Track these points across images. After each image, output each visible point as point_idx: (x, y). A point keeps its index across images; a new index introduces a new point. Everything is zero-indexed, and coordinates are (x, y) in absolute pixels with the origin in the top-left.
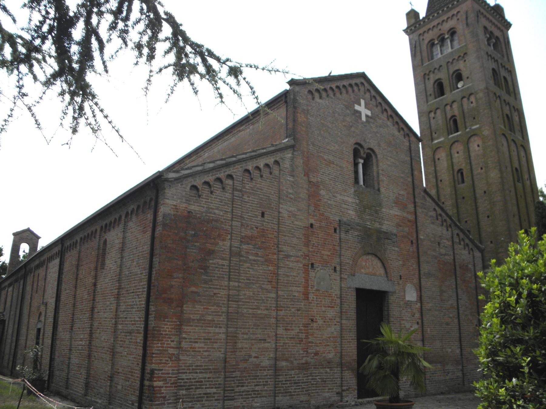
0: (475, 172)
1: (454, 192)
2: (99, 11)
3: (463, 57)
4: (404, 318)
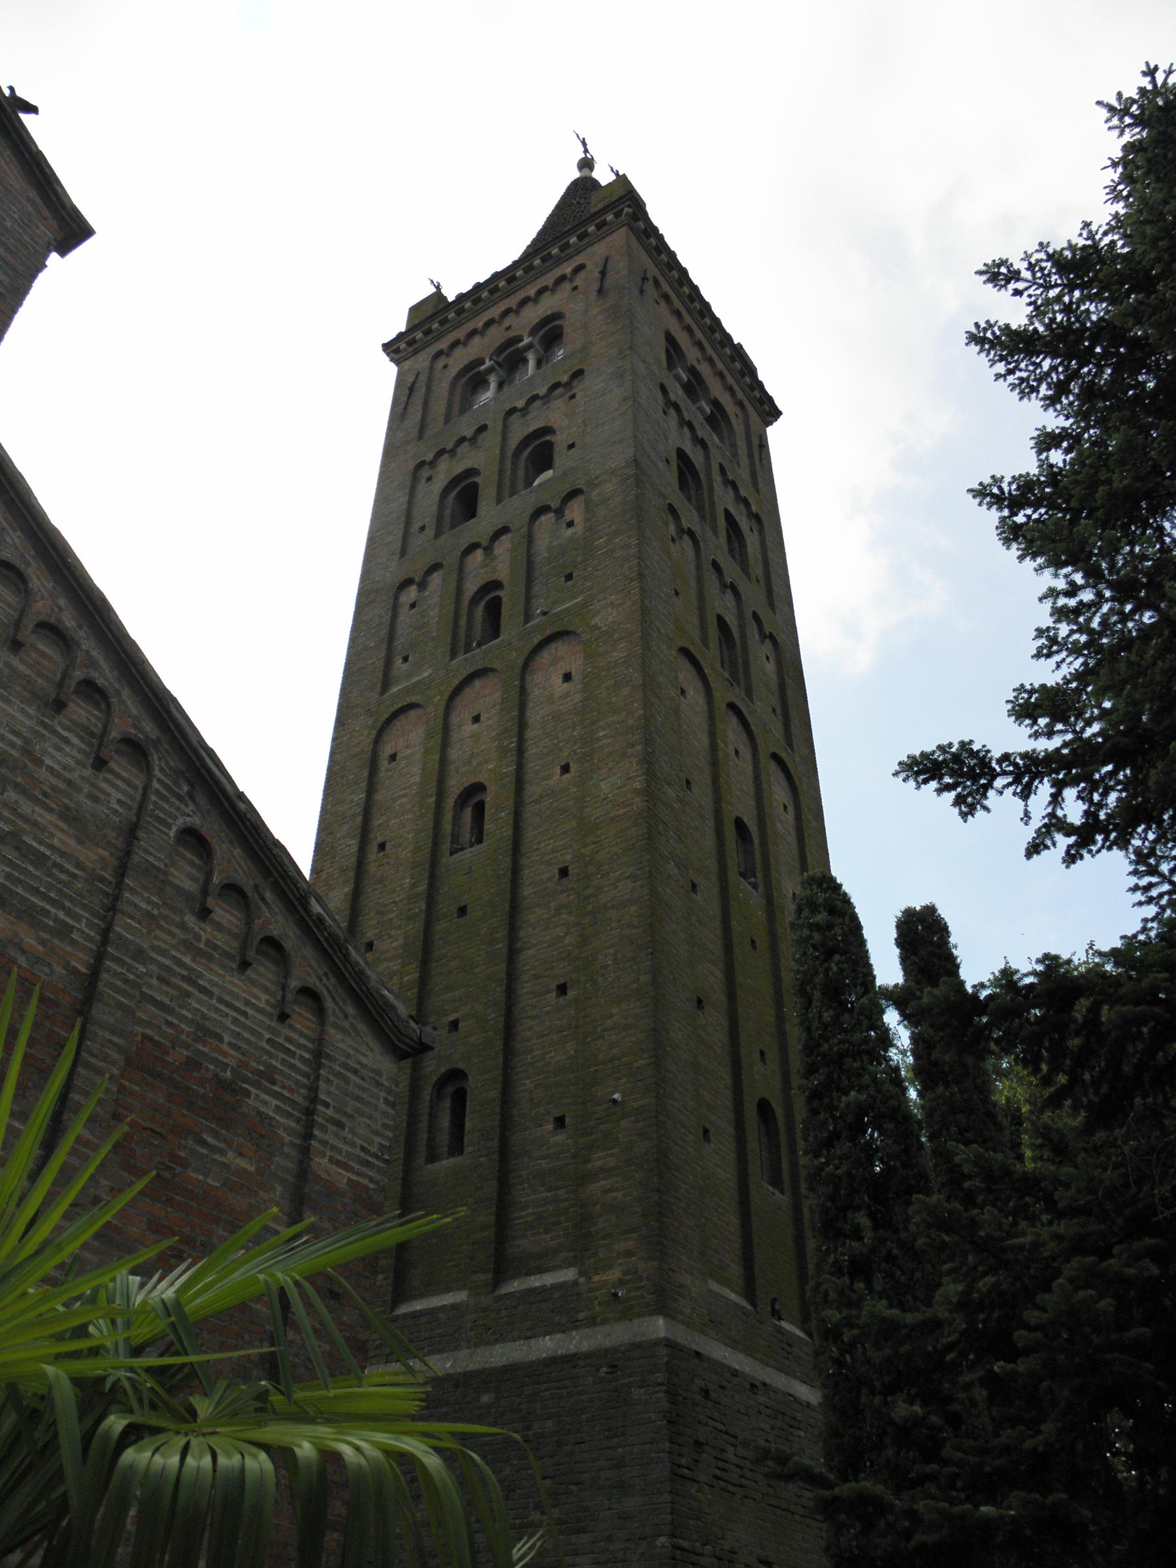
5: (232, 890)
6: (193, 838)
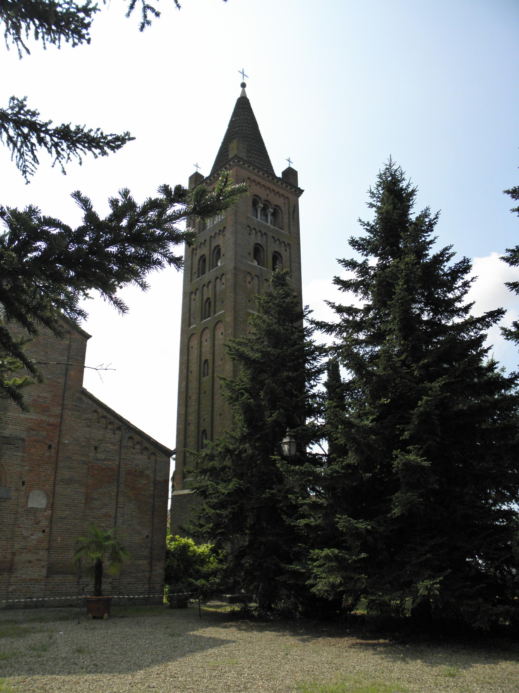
0: (216, 364)
1: (198, 386)
2: (28, 135)
3: (223, 231)
4: (21, 526)
5: (138, 443)
6: (131, 438)
